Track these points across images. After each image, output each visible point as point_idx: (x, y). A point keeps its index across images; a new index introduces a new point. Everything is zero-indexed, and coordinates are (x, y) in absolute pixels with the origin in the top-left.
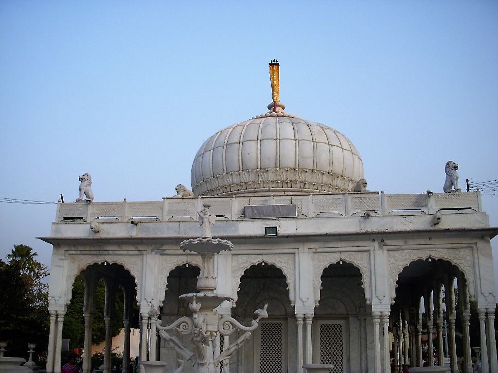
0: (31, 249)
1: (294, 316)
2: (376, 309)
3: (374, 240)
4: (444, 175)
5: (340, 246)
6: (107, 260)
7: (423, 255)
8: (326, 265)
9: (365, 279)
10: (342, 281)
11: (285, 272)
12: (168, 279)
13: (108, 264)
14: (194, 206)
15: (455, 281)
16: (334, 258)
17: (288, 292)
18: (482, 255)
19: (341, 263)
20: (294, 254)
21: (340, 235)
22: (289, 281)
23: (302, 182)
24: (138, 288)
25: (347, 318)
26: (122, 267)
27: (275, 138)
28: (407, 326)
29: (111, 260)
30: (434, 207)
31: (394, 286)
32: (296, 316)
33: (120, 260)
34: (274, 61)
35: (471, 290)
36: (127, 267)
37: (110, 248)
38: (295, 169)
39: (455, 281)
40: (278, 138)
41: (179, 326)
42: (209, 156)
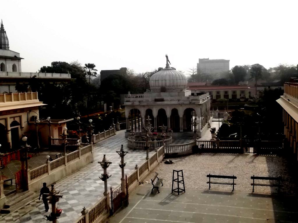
8: (172, 109)
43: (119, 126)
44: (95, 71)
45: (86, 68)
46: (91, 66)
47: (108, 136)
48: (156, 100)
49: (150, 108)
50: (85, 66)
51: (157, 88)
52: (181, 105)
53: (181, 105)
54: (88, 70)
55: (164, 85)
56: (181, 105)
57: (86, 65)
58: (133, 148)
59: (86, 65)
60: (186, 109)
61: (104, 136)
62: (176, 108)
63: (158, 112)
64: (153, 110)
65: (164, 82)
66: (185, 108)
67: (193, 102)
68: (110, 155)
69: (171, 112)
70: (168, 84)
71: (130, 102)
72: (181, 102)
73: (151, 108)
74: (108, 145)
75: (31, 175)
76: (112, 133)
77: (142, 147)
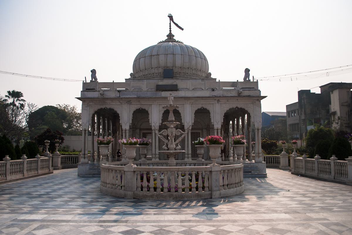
0: (22, 96)
1: (213, 128)
2: (216, 127)
3: (215, 100)
4: (244, 74)
5: (202, 101)
6: (106, 107)
7: (234, 106)
8: (196, 109)
9: (212, 115)
10: (202, 114)
11: (180, 111)
12: (133, 114)
13: (107, 108)
14: (143, 84)
15: (246, 115)
16: (199, 107)
17: (181, 119)
18: (257, 107)
19: (202, 108)
20: (184, 104)
21: (202, 97)
22: (182, 115)
23: (184, 73)
24: (120, 118)
25: (202, 130)
26: (113, 110)
27: (176, 55)
28: (223, 134)
29: (108, 107)
30: (240, 87)
31: (223, 118)
32: (214, 128)
33: (112, 107)
34: (170, 14)
35: (252, 120)
36: (115, 109)
37: (108, 102)
38: (181, 67)
39: (246, 115)
40: (174, 54)
41: (163, 133)
42: (142, 60)
43: (60, 159)
44: (22, 102)
45: (8, 97)
46: (16, 95)
47: (33, 173)
48: (160, 88)
49: (144, 107)
50: (7, 94)
51: (153, 71)
52: (218, 99)
53: (218, 101)
54: (10, 100)
55: (170, 65)
56: (218, 99)
57: (9, 92)
58: (130, 193)
59: (9, 92)
60: (228, 109)
61: (22, 172)
62: (205, 107)
63: (161, 115)
64: (149, 112)
65: (170, 58)
66: (226, 107)
67: (246, 93)
68: (36, 225)
69: (193, 115)
70: (179, 63)
71: (96, 91)
72: (215, 93)
73: (145, 107)
74: (33, 190)
75: (250, 177)
76: (42, 168)
77: (166, 190)
